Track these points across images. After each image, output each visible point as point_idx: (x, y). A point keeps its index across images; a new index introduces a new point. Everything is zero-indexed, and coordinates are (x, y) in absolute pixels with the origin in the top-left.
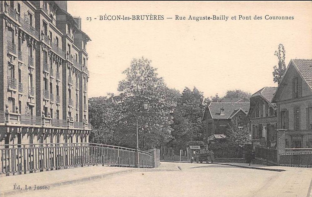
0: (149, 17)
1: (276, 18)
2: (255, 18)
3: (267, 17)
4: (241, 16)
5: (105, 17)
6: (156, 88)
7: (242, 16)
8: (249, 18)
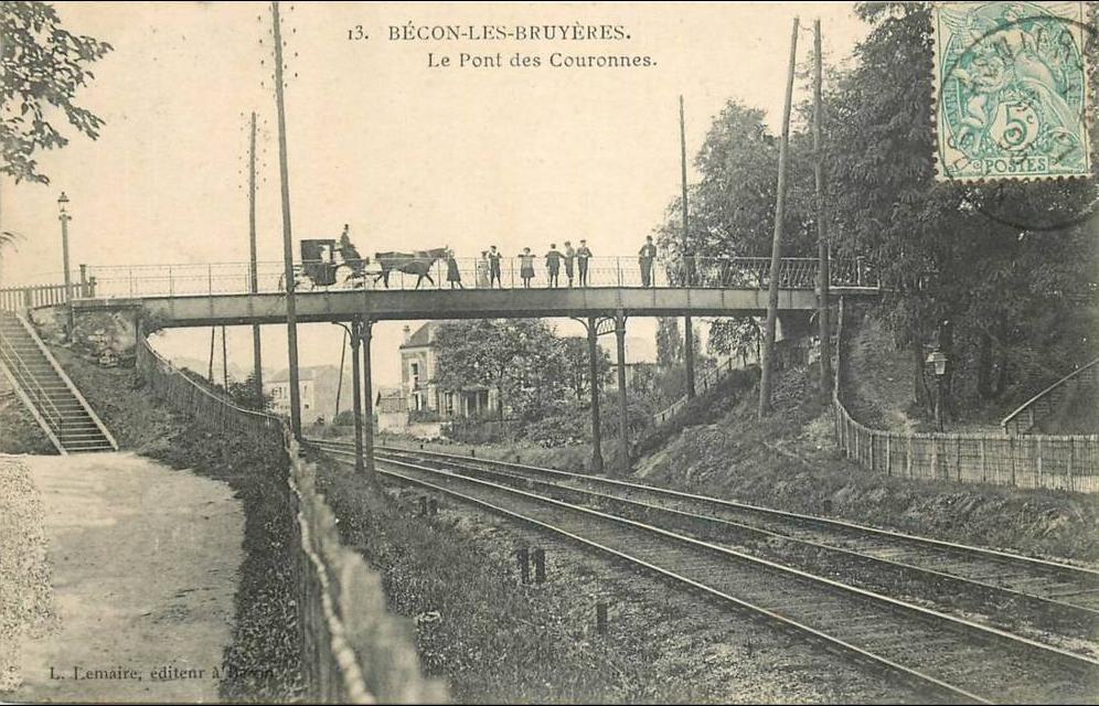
0: (571, 30)
1: (587, 61)
2: (515, 62)
3: (557, 60)
4: (465, 57)
5: (408, 30)
6: (1029, 619)
7: (572, 59)
8: (495, 62)
